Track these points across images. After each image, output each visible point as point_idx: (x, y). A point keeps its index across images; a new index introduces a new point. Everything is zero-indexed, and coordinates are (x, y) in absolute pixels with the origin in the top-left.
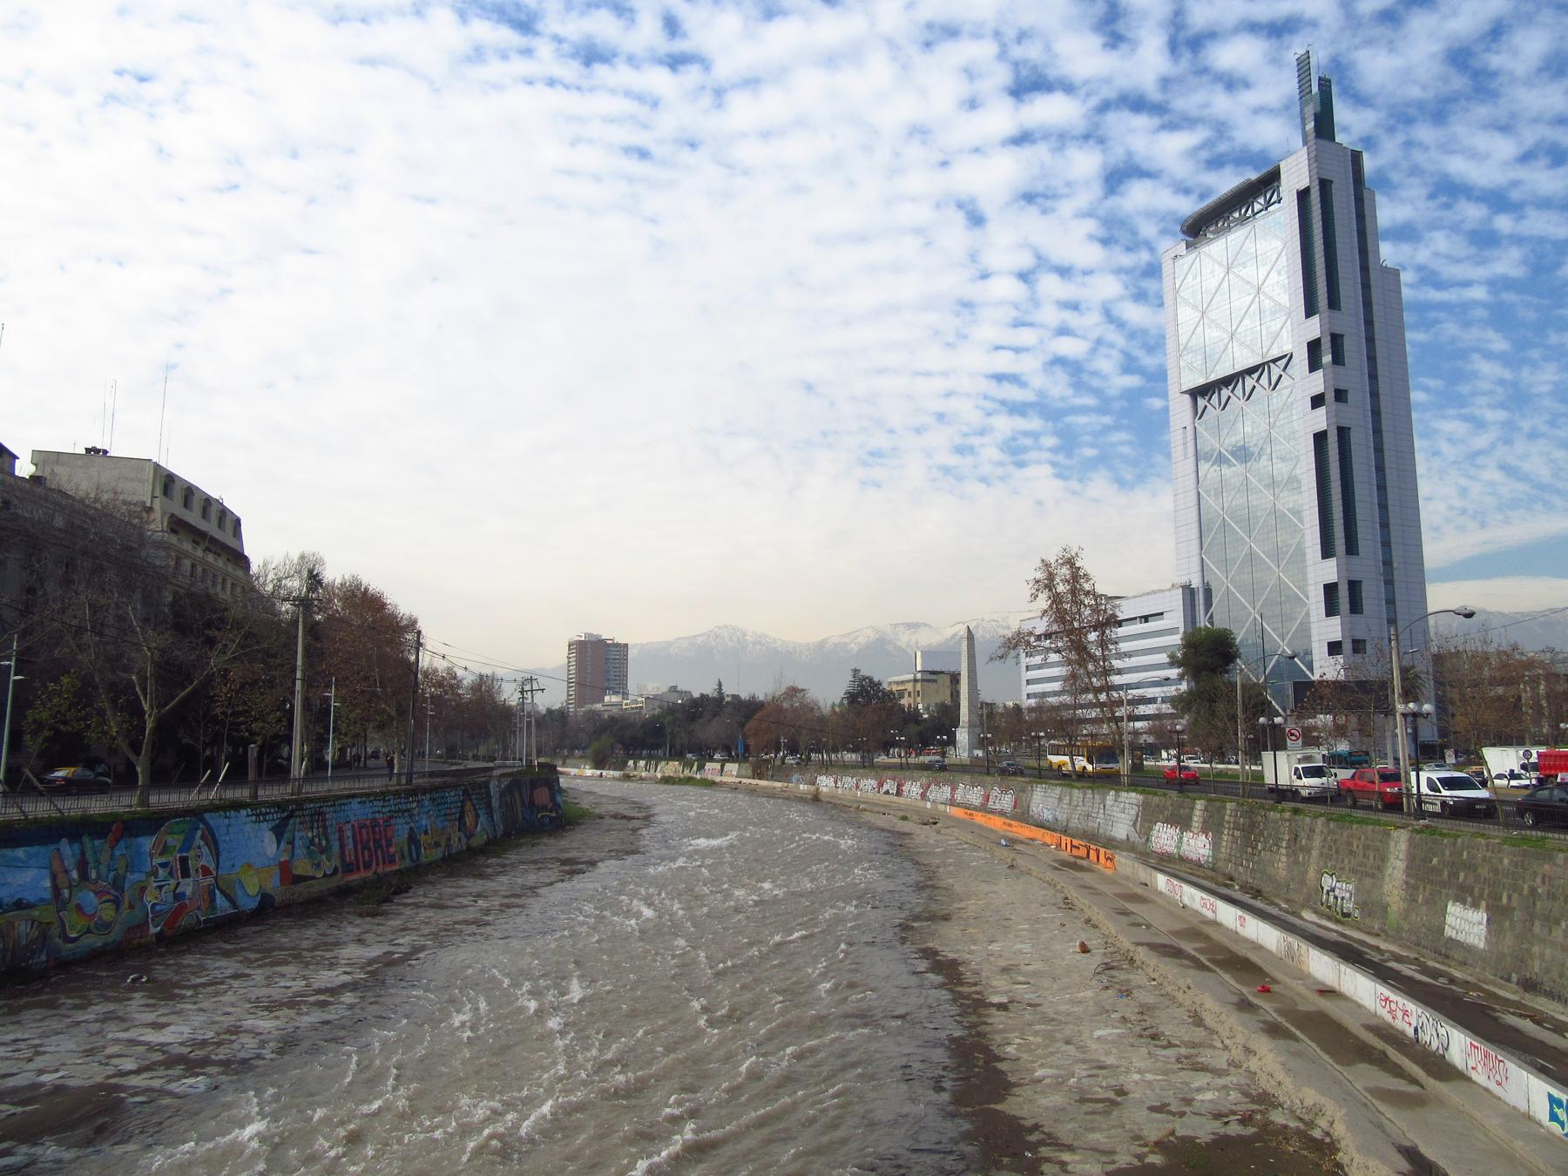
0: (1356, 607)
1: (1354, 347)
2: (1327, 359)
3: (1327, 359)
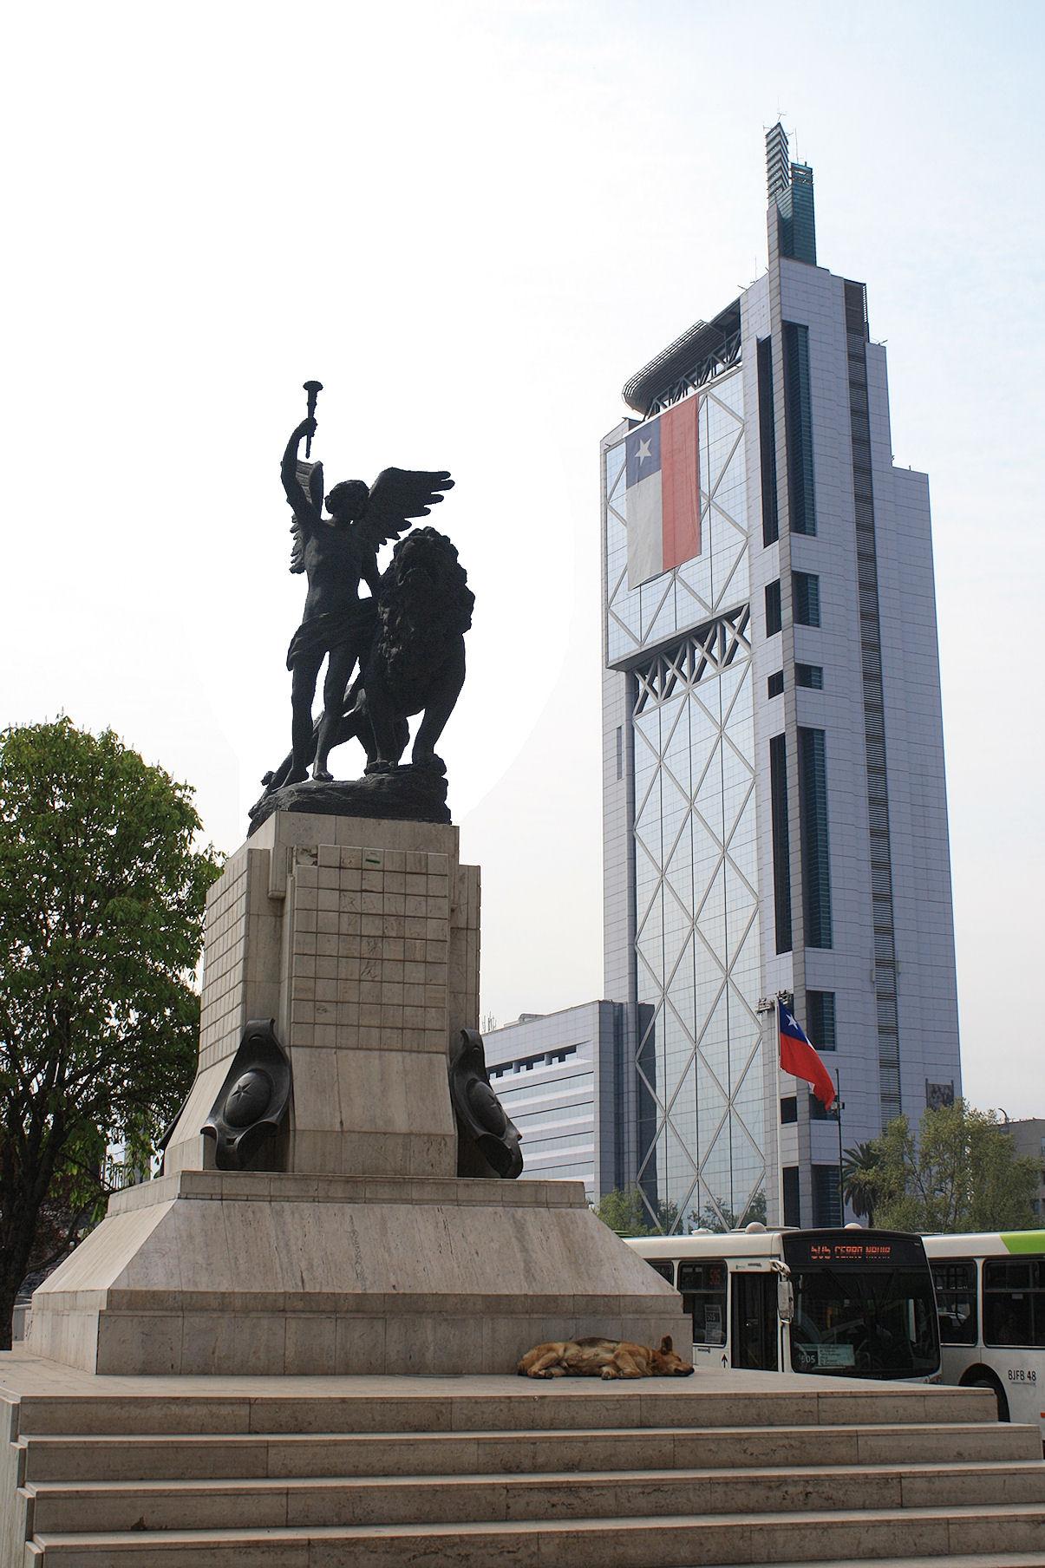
0: (806, 613)
1: (838, 598)
2: (787, 614)
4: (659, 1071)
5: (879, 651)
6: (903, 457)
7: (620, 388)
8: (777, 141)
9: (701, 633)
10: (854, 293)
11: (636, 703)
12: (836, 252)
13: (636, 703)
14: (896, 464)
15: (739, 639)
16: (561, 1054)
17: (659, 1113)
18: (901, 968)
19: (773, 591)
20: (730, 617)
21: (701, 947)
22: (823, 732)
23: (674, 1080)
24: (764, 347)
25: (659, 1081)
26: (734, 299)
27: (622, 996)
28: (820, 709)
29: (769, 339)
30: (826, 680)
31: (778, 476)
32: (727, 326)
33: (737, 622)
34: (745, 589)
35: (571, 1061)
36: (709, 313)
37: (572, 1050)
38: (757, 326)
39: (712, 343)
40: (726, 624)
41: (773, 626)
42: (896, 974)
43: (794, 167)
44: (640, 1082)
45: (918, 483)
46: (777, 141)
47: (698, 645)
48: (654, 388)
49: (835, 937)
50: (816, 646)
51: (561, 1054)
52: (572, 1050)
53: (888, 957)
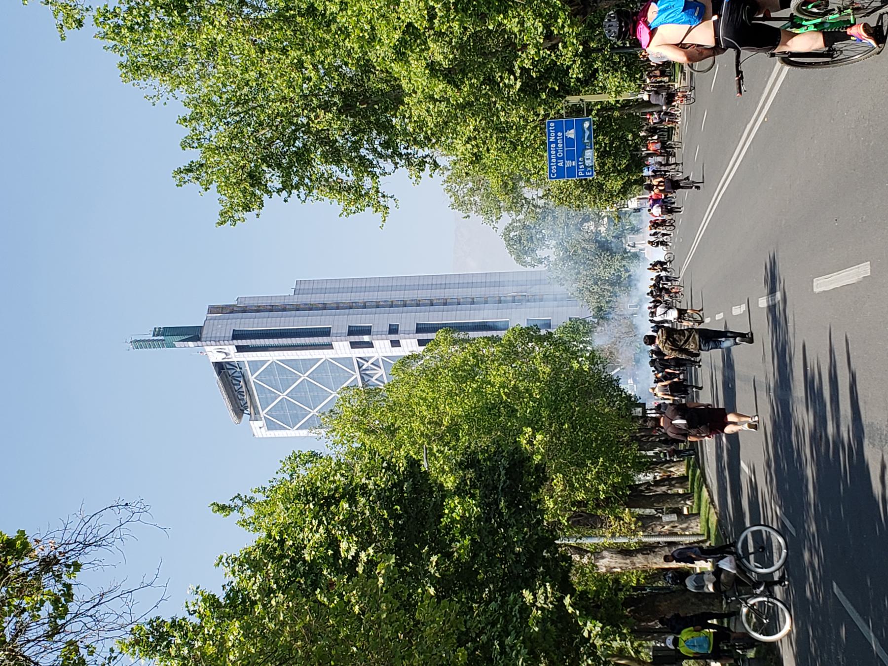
0: (367, 331)
1: (360, 320)
2: (366, 338)
3: (366, 338)
8: (139, 344)
10: (212, 310)
29: (237, 347)
46: (139, 344)
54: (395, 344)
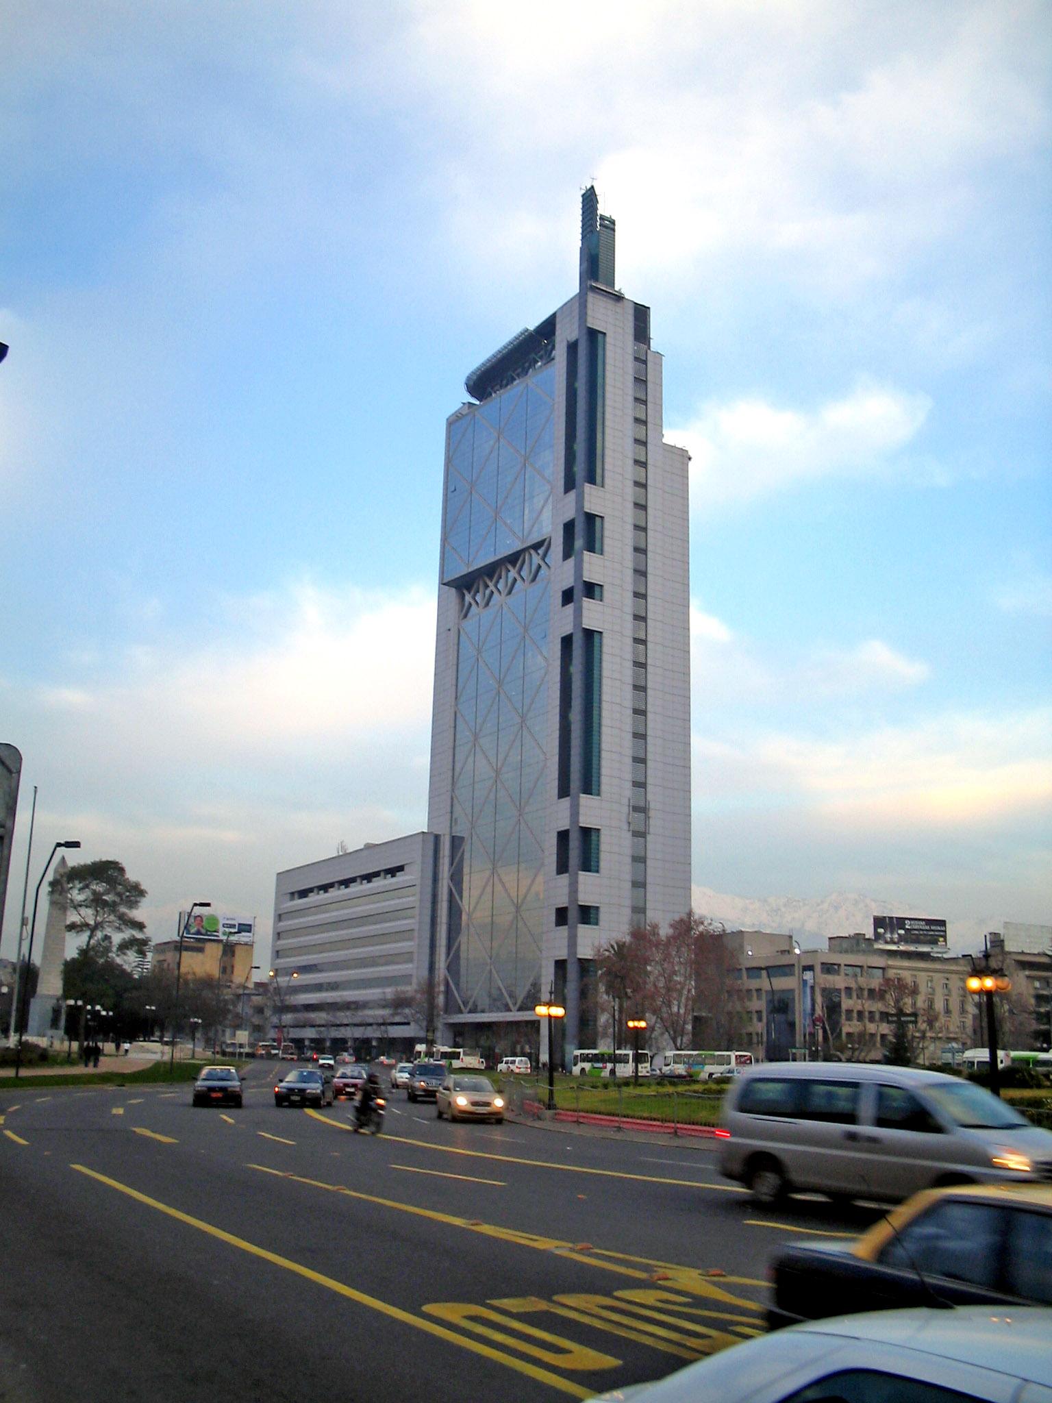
0: (589, 863)
1: (614, 848)
2: (579, 543)
4: (465, 885)
5: (645, 862)
6: (672, 436)
7: (463, 380)
8: (590, 199)
9: (514, 559)
10: (641, 314)
11: (465, 612)
12: (630, 277)
13: (465, 612)
14: (664, 441)
15: (542, 563)
16: (393, 872)
17: (464, 917)
18: (652, 813)
19: (569, 527)
20: (536, 547)
21: (499, 887)
22: (598, 830)
23: (475, 893)
24: (572, 347)
25: (465, 894)
26: (551, 313)
27: (444, 830)
28: (593, 614)
30: (606, 594)
31: (572, 769)
32: (548, 328)
33: (541, 551)
34: (550, 526)
35: (400, 878)
36: (533, 324)
37: (400, 868)
38: (565, 333)
39: (531, 348)
40: (532, 552)
41: (568, 553)
42: (647, 818)
43: (602, 218)
44: (451, 894)
45: (683, 457)
46: (590, 199)
47: (510, 567)
48: (485, 383)
49: (602, 864)
50: (593, 568)
51: (393, 872)
52: (400, 868)
53: (642, 731)
54: (568, 597)
